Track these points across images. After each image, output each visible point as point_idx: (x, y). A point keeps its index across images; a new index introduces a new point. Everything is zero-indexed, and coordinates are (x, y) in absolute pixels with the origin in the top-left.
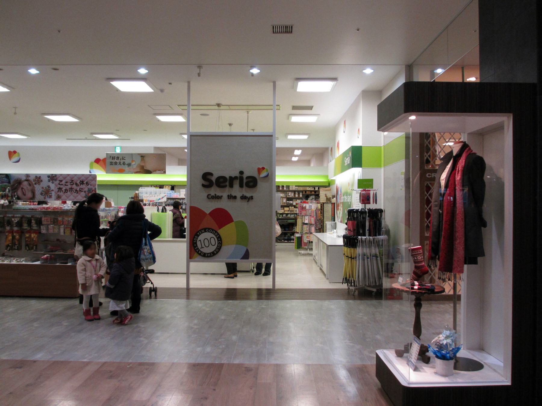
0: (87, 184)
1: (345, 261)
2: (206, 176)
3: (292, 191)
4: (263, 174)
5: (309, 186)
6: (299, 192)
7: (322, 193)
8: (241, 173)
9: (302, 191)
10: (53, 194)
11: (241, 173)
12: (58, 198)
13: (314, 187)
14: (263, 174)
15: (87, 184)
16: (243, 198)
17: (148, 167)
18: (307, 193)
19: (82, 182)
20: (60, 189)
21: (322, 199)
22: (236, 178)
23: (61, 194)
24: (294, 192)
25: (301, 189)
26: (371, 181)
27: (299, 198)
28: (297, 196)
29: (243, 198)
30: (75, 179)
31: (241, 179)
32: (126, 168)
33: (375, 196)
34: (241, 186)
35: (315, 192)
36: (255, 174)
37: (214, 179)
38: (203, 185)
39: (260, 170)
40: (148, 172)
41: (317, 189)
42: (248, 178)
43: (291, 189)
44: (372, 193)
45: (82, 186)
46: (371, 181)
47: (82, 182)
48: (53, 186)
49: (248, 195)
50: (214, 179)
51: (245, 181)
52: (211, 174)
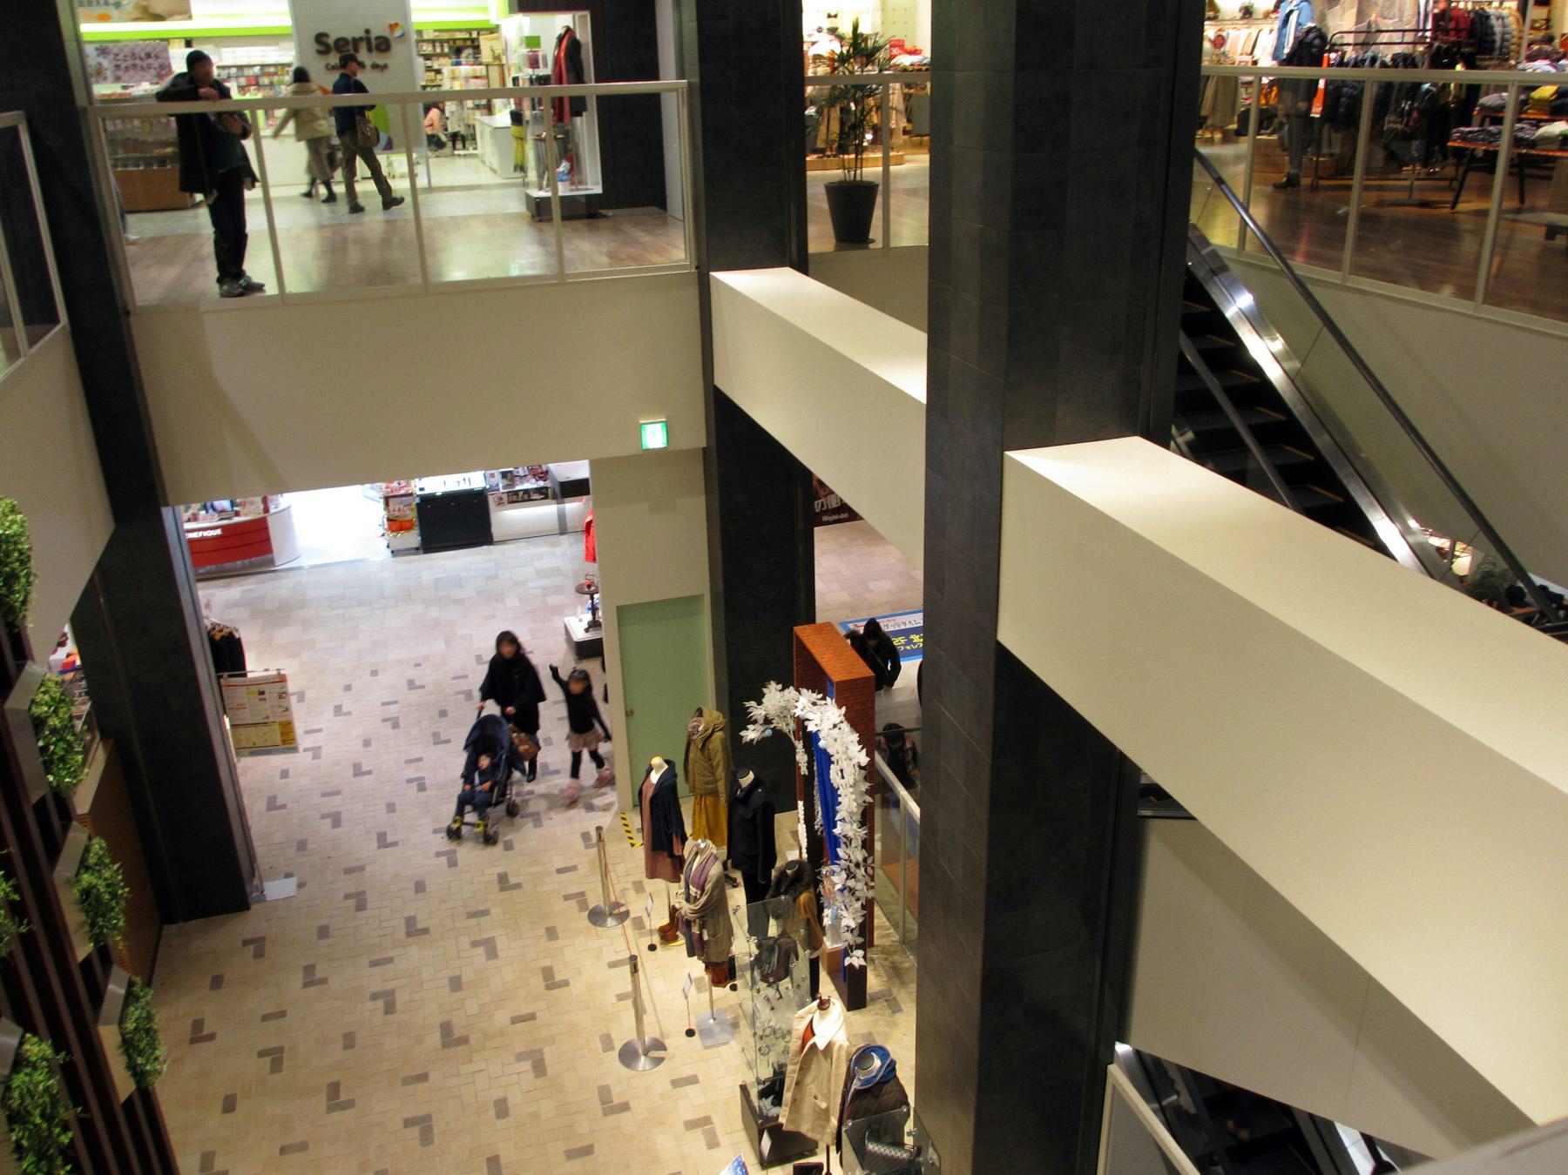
0: (157, 57)
1: (514, 143)
2: (320, 38)
3: (427, 41)
4: (398, 33)
5: (461, 31)
6: (442, 42)
7: (485, 44)
8: (368, 31)
9: (447, 41)
10: (109, 74)
11: (368, 31)
12: (118, 79)
13: (469, 31)
14: (398, 33)
15: (157, 57)
16: (375, 66)
17: (158, 10)
18: (459, 43)
19: (148, 56)
20: (117, 67)
21: (486, 56)
22: (361, 39)
23: (120, 73)
24: (433, 42)
25: (446, 36)
26: (538, 38)
27: (443, 55)
28: (438, 50)
29: (375, 66)
30: (137, 51)
31: (368, 40)
32: (112, 11)
33: (545, 58)
34: (370, 50)
35: (473, 40)
36: (386, 33)
37: (331, 41)
38: (319, 52)
39: (393, 27)
40: (158, 18)
41: (474, 35)
42: (378, 38)
43: (426, 37)
44: (540, 55)
45: (150, 61)
46: (538, 38)
47: (148, 56)
48: (106, 63)
49: (381, 62)
50: (331, 41)
51: (374, 43)
52: (326, 35)
